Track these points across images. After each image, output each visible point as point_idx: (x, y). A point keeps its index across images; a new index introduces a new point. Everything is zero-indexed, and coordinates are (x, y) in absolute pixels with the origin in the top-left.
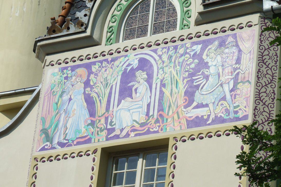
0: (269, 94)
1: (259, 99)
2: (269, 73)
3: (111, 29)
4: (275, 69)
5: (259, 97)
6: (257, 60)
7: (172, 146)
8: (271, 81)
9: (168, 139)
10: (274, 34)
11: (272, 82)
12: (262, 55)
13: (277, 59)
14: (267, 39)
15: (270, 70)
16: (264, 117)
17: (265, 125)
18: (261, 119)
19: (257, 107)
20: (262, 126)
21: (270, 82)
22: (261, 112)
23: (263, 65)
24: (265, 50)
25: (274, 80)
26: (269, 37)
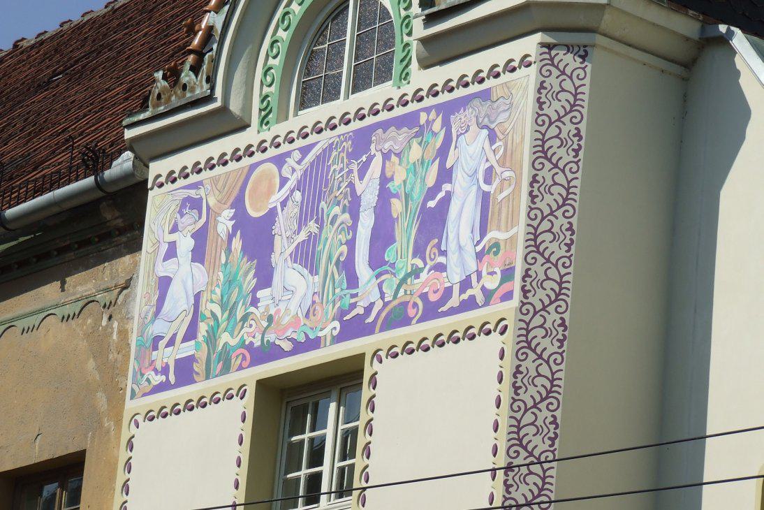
0: (542, 427)
1: (535, 249)
2: (566, 89)
3: (265, 103)
4: (559, 361)
5: (543, 151)
6: (530, 151)
7: (360, 471)
8: (549, 392)
9: (362, 356)
10: (565, 175)
11: (550, 395)
12: (528, 327)
13: (579, 145)
14: (554, 97)
15: (554, 268)
16: (529, 487)
17: (540, 411)
18: (532, 396)
19: (544, 82)
20: (541, 316)
21: (544, 395)
22: (522, 477)
23: (521, 452)
24: (535, 313)
25: (547, 486)
26: (545, 280)
